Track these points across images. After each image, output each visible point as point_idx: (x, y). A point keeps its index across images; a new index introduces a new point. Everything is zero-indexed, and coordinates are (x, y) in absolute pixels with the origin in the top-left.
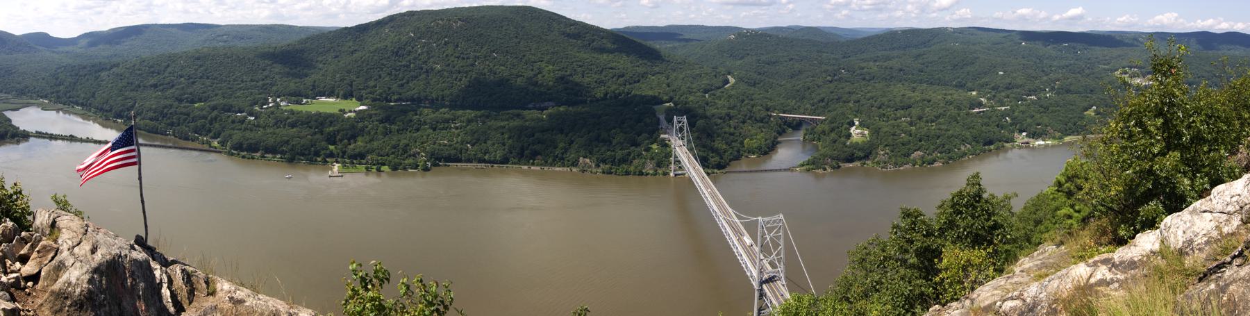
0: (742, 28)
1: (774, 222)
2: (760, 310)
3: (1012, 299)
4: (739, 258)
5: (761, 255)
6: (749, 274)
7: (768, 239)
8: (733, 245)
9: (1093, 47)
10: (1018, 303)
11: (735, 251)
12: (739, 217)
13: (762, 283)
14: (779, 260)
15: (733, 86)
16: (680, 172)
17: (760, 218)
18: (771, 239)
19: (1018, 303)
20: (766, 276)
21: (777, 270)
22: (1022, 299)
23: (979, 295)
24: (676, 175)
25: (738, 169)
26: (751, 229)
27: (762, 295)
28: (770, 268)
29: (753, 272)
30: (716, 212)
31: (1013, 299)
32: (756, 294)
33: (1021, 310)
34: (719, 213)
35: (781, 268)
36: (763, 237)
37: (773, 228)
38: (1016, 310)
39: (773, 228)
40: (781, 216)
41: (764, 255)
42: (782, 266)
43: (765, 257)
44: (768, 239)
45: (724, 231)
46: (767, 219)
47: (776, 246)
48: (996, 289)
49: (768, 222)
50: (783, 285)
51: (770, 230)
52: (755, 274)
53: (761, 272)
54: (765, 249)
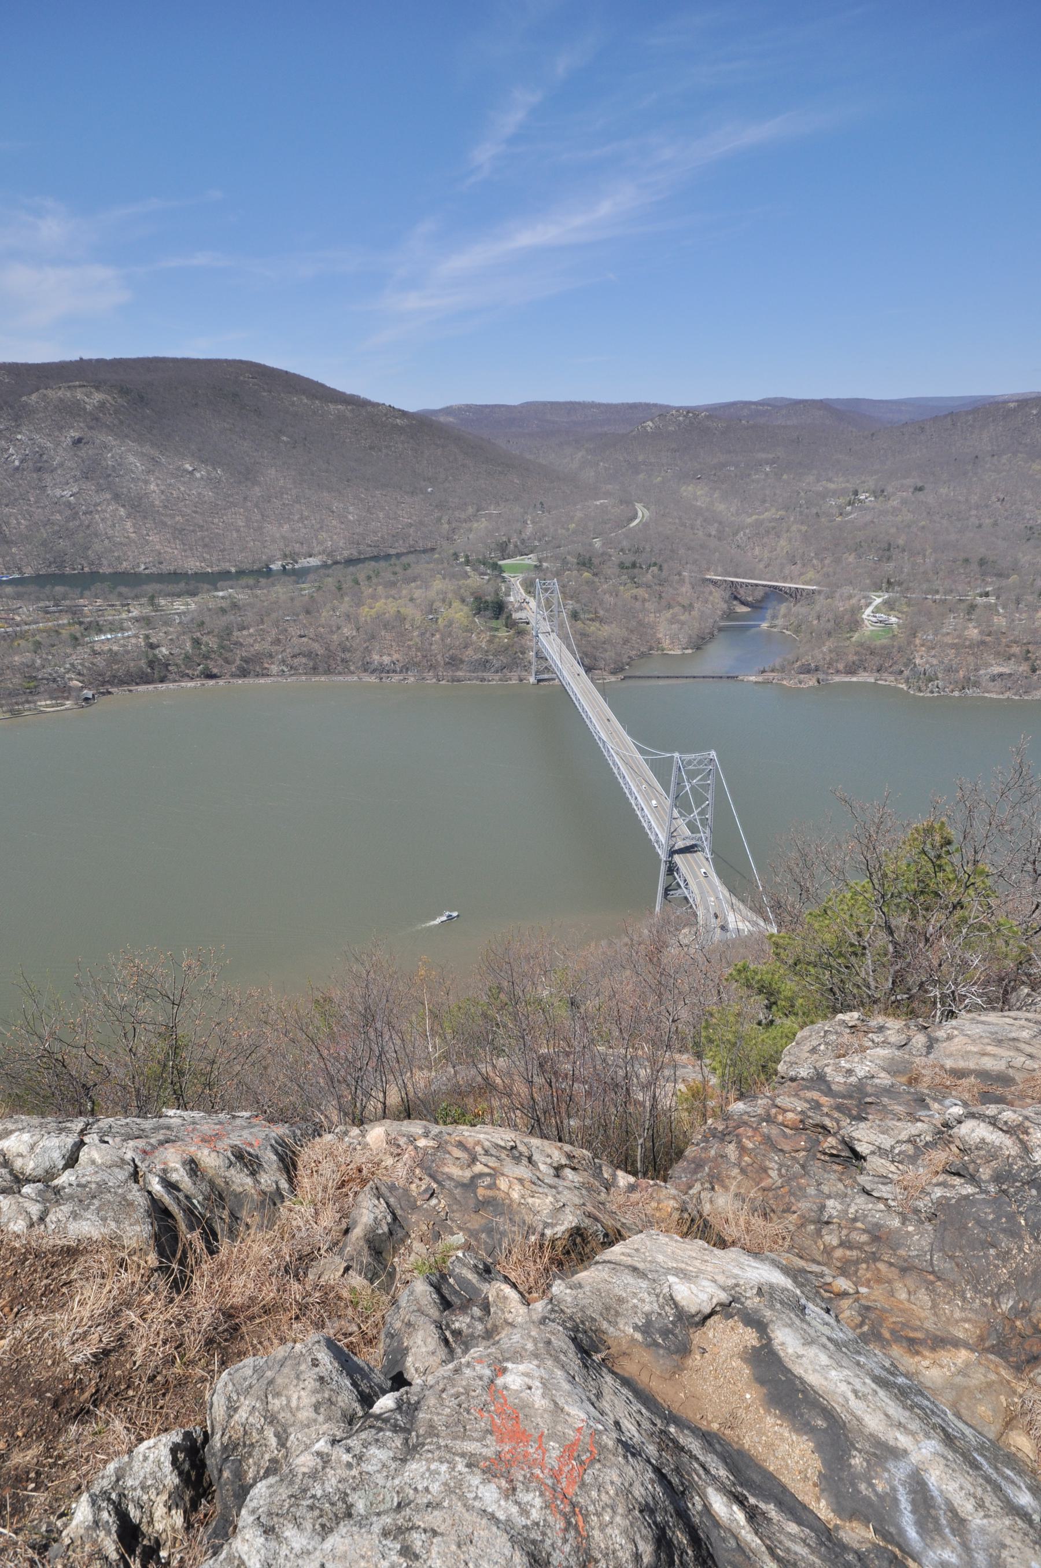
0: (668, 406)
1: (700, 762)
2: (667, 890)
3: (993, 1122)
4: (638, 813)
5: (675, 811)
6: (653, 838)
7: (688, 788)
8: (631, 793)
9: (936, 1493)
10: (1008, 1145)
11: (633, 802)
12: (642, 752)
13: (672, 853)
14: (704, 822)
15: (645, 525)
16: (546, 676)
17: (676, 755)
18: (692, 788)
19: (1008, 1145)
20: (680, 844)
21: (698, 835)
22: (1021, 1141)
23: (949, 1038)
24: (539, 681)
25: (638, 674)
26: (662, 770)
27: (672, 869)
28: (688, 832)
29: (659, 835)
30: (604, 742)
31: (994, 1125)
32: (663, 868)
33: (1010, 1165)
34: (609, 745)
35: (704, 835)
36: (679, 784)
37: (697, 772)
38: (995, 1157)
39: (697, 772)
40: (713, 754)
41: (679, 812)
42: (708, 831)
43: (682, 815)
44: (688, 788)
45: (615, 771)
46: (688, 757)
47: (700, 800)
48: (999, 1042)
49: (690, 763)
50: (707, 859)
51: (692, 775)
52: (662, 839)
53: (671, 835)
54: (681, 803)
